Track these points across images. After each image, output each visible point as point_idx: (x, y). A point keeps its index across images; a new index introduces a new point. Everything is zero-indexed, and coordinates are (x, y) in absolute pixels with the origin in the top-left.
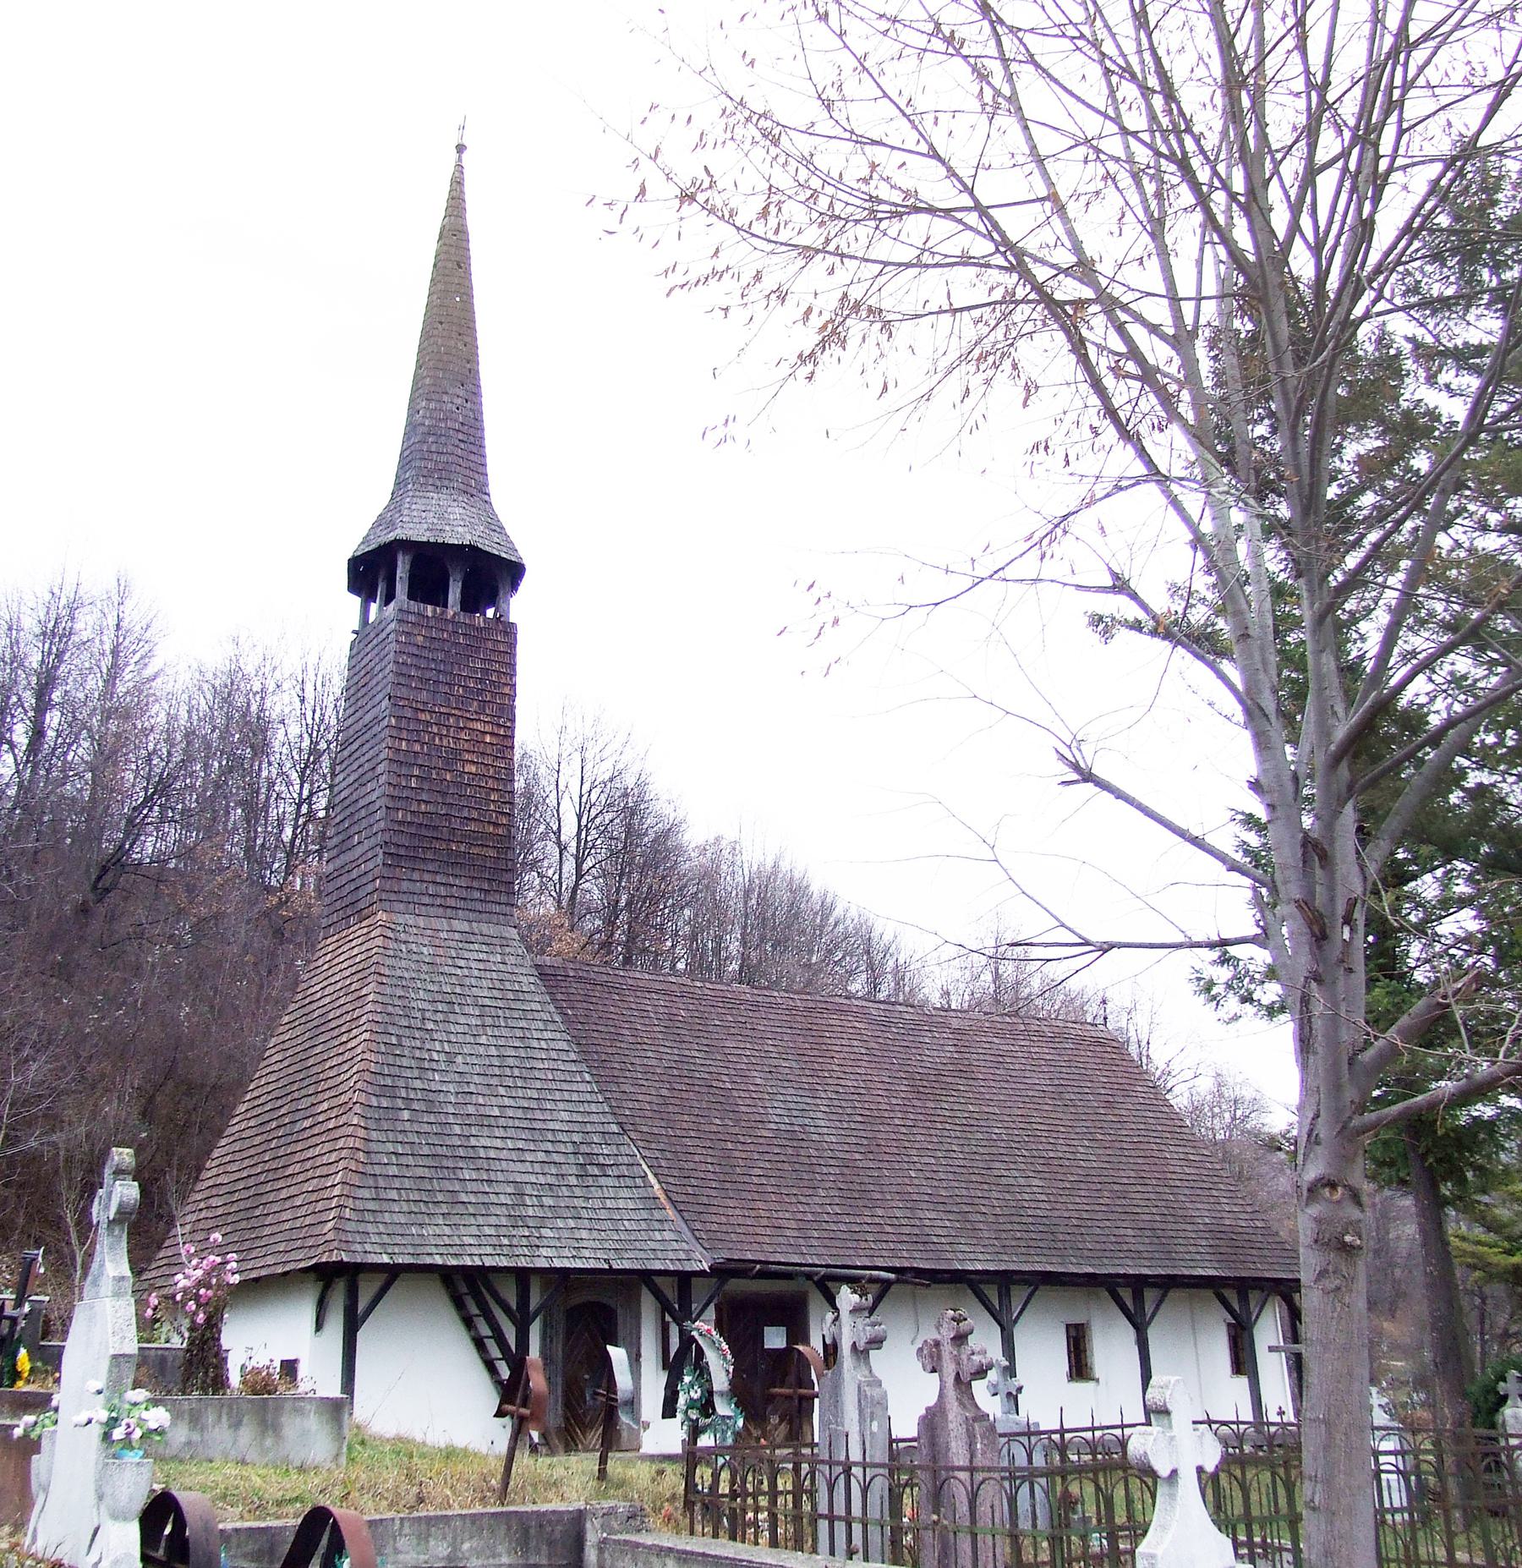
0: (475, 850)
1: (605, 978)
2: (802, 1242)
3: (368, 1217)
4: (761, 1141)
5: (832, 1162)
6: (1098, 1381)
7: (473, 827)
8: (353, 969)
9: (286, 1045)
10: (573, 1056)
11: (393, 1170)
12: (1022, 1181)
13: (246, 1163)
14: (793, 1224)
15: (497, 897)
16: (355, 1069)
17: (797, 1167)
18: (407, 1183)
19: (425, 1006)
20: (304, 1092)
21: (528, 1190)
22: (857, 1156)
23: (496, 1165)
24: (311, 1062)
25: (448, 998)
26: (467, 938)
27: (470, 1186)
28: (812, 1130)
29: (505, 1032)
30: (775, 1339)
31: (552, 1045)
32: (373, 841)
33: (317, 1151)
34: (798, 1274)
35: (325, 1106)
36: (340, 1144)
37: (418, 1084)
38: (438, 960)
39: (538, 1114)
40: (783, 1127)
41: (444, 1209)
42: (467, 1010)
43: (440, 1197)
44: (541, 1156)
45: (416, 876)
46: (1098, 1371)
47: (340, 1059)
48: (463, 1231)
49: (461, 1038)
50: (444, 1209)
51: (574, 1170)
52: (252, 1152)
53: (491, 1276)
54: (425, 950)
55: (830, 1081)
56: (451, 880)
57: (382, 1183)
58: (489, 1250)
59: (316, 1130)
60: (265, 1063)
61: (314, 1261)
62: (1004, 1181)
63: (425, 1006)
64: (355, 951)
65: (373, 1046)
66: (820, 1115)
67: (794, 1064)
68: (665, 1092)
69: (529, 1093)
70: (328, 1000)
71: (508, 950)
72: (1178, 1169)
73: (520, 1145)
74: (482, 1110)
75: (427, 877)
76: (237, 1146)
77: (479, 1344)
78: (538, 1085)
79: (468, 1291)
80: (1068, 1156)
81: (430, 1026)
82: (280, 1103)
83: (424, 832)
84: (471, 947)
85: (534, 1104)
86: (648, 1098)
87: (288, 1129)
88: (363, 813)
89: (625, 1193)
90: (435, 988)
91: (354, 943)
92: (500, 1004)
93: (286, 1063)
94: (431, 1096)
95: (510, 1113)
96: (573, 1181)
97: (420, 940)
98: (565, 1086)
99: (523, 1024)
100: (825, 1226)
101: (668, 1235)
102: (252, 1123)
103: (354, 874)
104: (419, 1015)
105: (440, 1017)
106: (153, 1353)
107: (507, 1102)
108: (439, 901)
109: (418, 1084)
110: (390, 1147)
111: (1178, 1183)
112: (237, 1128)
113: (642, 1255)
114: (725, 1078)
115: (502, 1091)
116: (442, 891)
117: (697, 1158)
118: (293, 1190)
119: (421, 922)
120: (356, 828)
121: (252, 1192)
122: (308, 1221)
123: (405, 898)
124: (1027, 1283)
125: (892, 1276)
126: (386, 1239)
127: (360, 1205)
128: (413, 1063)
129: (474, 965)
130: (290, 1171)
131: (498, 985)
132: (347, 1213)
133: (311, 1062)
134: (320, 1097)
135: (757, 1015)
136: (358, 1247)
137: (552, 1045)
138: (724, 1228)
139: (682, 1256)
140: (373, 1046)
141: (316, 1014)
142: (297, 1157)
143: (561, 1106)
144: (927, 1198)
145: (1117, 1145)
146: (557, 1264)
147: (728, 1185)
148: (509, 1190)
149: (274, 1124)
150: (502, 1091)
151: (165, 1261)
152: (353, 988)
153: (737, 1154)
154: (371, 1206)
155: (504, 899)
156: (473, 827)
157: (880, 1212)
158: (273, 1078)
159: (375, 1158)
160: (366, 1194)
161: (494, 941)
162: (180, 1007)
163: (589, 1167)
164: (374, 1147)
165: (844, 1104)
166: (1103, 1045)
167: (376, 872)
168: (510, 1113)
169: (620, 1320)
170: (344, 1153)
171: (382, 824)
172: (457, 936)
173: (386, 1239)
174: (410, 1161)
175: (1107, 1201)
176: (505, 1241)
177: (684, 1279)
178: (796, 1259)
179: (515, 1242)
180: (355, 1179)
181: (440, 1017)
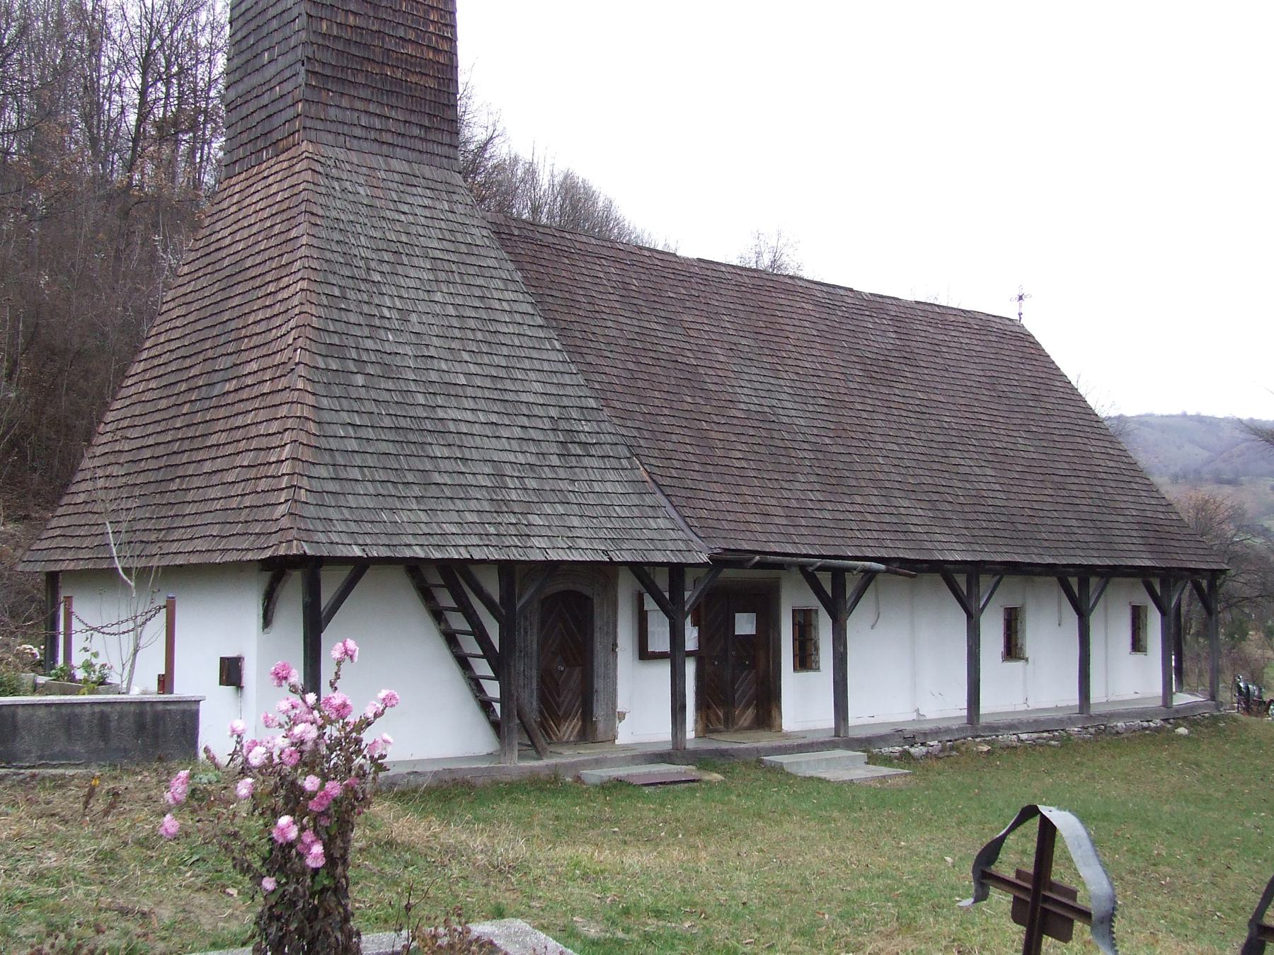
0: (414, 79)
1: (551, 240)
2: (792, 530)
3: (328, 500)
4: (735, 421)
5: (806, 446)
6: (1027, 660)
7: (410, 50)
8: (274, 209)
9: (189, 298)
10: (540, 321)
11: (353, 445)
12: (978, 471)
13: (150, 429)
14: (780, 511)
15: (438, 137)
16: (292, 324)
17: (774, 450)
18: (370, 461)
19: (369, 254)
20: (220, 351)
21: (508, 470)
22: (827, 441)
23: (468, 441)
24: (226, 316)
25: (393, 247)
26: (408, 181)
27: (443, 465)
28: (781, 411)
29: (461, 289)
30: (745, 625)
31: (516, 307)
32: (291, 57)
33: (249, 419)
34: (791, 565)
35: (254, 366)
36: (283, 411)
37: (369, 344)
38: (378, 203)
39: (509, 385)
40: (753, 408)
41: (417, 491)
42: (416, 261)
43: (410, 477)
44: (518, 432)
45: (345, 102)
46: (1028, 652)
47: (269, 313)
48: (441, 517)
49: (413, 294)
50: (417, 491)
51: (554, 449)
52: (157, 417)
53: (472, 568)
54: (361, 190)
55: (790, 362)
56: (386, 111)
57: (340, 460)
58: (476, 540)
59: (245, 394)
60: (164, 318)
61: (268, 554)
62: (961, 470)
63: (369, 254)
64: (274, 189)
65: (314, 298)
66: (785, 397)
67: (752, 343)
68: (631, 366)
69: (497, 360)
70: (241, 246)
71: (455, 197)
72: (1101, 462)
73: (494, 418)
74: (447, 378)
75: (359, 105)
76: (137, 410)
77: (451, 638)
78: (505, 351)
79: (441, 586)
80: (1011, 446)
81: (377, 277)
82: (188, 362)
83: (354, 50)
84: (414, 190)
85: (502, 373)
86: (615, 371)
87: (204, 392)
88: (275, 24)
89: (612, 475)
90: (378, 234)
91: (271, 180)
92: (453, 257)
93: (191, 318)
94: (387, 359)
95: (478, 381)
96: (555, 461)
97: (354, 177)
98: (535, 354)
99: (480, 281)
100: (810, 513)
101: (662, 523)
102: (153, 384)
103: (266, 99)
104: (362, 263)
105: (386, 268)
106: (87, 710)
107: (473, 369)
108: (373, 135)
109: (369, 344)
110: (345, 417)
111: (1105, 476)
112: (133, 390)
113: (639, 545)
114: (689, 354)
115: (466, 356)
116: (377, 123)
117: (674, 438)
118: (219, 464)
119: (354, 158)
120: (266, 44)
121: (163, 462)
122: (248, 501)
123: (333, 127)
124: (995, 573)
125: (882, 567)
126: (354, 527)
127: (316, 485)
128: (362, 320)
129: (418, 211)
130: (213, 440)
131: (448, 235)
132: (303, 495)
133: (226, 316)
134: (245, 357)
135: (708, 289)
136: (322, 537)
137: (516, 307)
138: (715, 515)
139: (682, 546)
140: (314, 298)
141: (226, 262)
142: (221, 425)
143: (533, 376)
144: (897, 485)
145: (1048, 437)
146: (553, 556)
147: (710, 468)
148: (487, 470)
149: (184, 387)
150: (466, 356)
151: (58, 532)
152: (276, 230)
153: (713, 435)
154: (332, 486)
155: (447, 139)
156: (410, 50)
157: (858, 499)
158: (177, 334)
159: (329, 430)
160: (323, 472)
161: (439, 186)
162: (39, 274)
163: (571, 446)
164: (326, 416)
165: (805, 386)
166: (1021, 340)
167: (298, 94)
168: (478, 381)
169: (597, 610)
170: (289, 423)
171: (303, 36)
172: (397, 177)
173: (354, 527)
174: (371, 434)
175: (1051, 492)
176: (492, 530)
177: (677, 571)
178: (790, 549)
179: (502, 530)
180: (307, 455)
181: (386, 268)
